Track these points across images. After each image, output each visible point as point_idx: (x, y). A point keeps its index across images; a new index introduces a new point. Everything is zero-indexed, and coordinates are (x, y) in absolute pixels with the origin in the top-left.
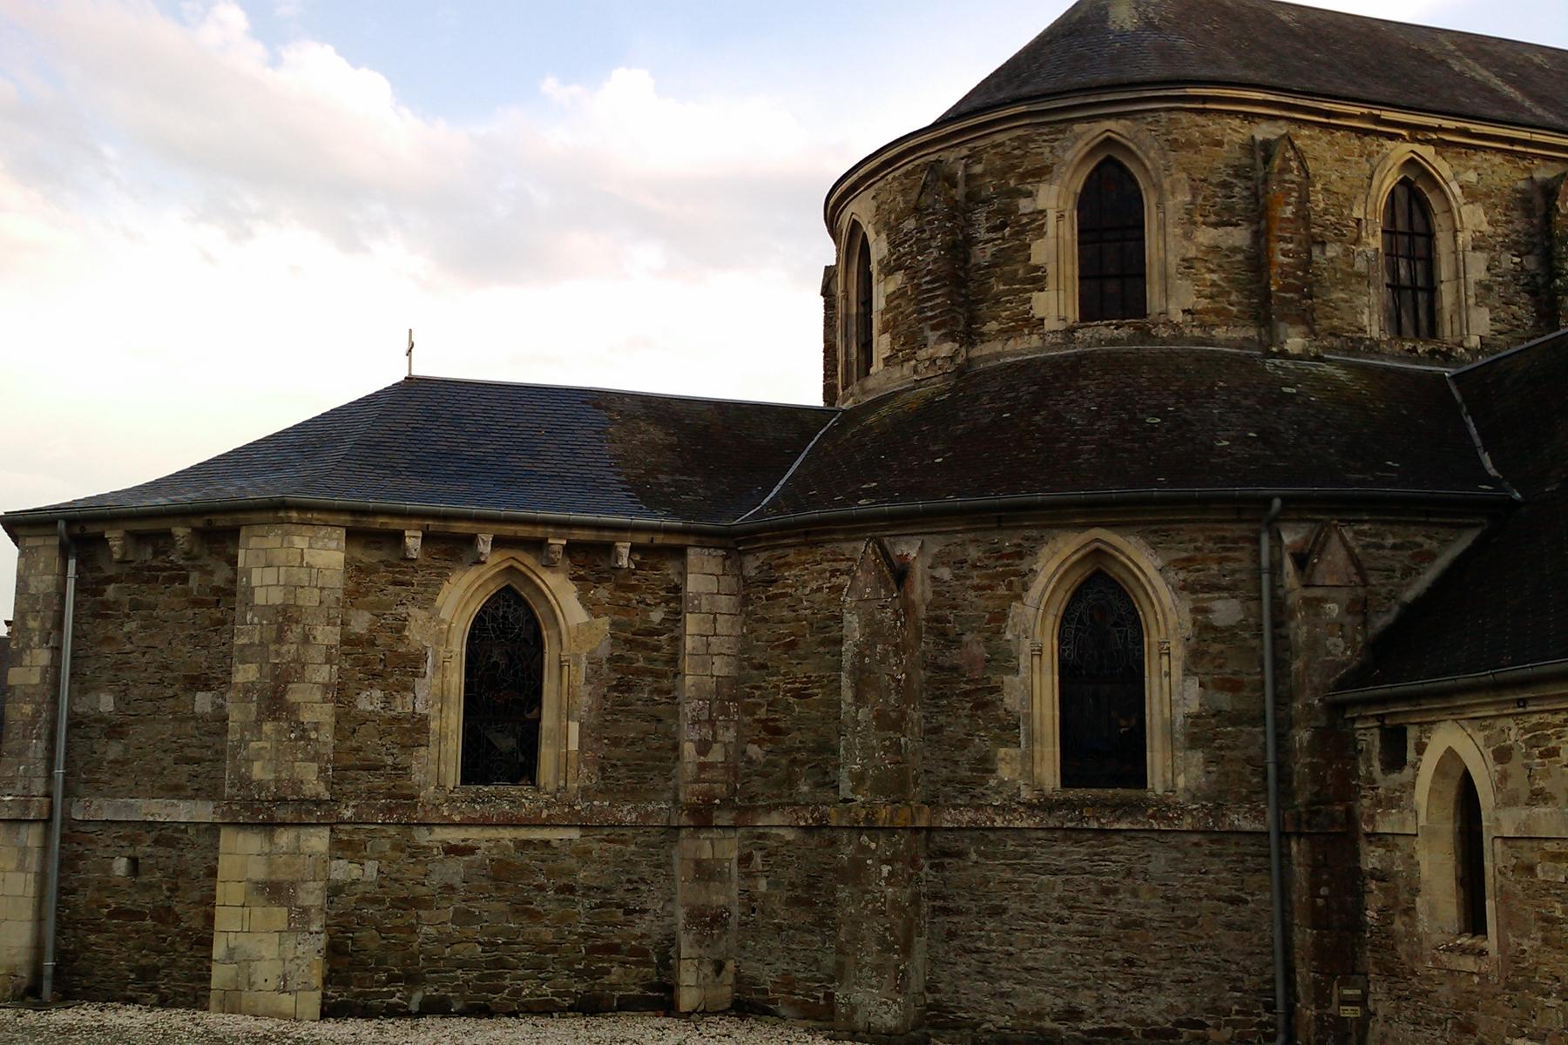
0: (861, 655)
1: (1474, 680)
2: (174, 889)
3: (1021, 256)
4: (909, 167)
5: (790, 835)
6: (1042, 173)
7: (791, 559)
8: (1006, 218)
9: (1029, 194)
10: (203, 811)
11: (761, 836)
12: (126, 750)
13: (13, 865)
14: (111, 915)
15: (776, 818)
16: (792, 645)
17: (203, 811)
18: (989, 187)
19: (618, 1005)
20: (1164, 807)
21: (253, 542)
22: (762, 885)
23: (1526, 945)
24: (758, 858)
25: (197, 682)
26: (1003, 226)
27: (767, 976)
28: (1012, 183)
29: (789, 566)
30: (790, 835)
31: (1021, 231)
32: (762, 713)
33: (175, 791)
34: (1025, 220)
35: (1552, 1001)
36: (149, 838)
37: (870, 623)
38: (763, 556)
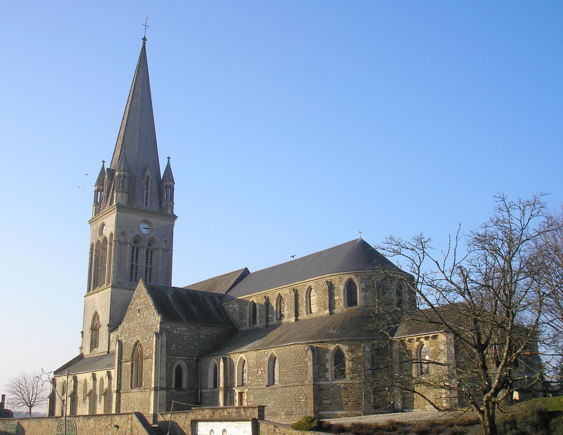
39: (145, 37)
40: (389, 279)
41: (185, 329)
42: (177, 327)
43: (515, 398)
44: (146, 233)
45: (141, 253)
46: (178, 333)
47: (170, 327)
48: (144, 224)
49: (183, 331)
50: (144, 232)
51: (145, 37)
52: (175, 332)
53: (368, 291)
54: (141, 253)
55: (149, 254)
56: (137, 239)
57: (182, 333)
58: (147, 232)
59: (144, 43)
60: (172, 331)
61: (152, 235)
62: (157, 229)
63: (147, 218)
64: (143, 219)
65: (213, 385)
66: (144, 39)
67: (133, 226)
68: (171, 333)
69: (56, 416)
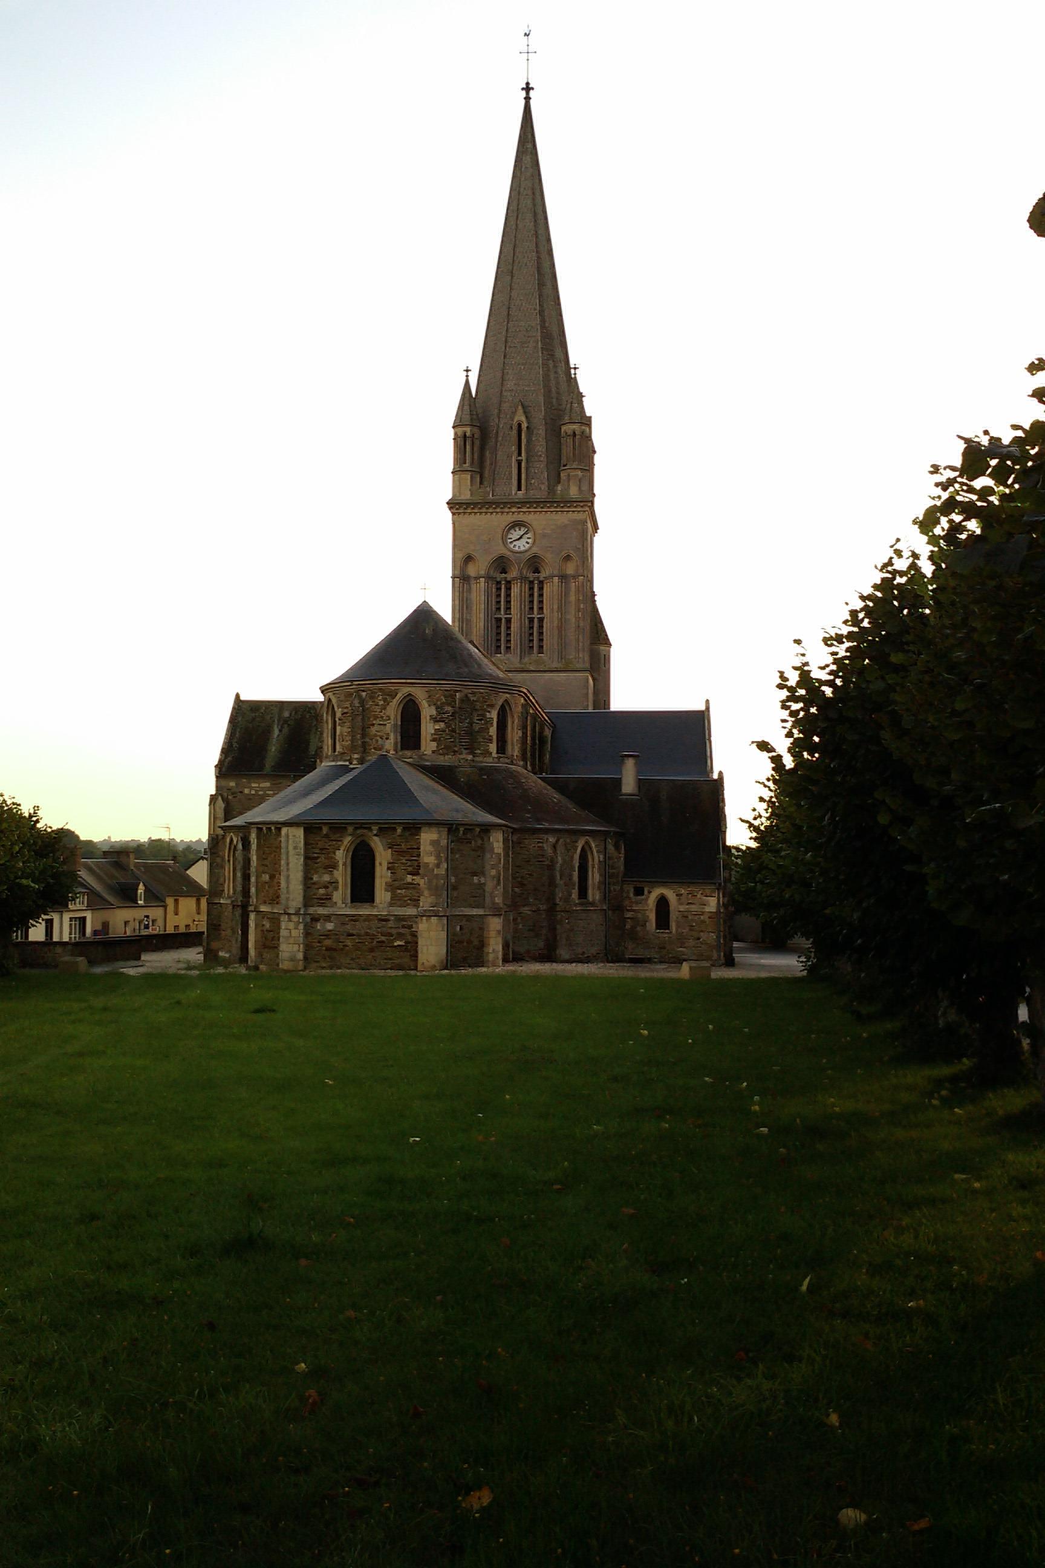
0: (561, 867)
1: (596, 870)
2: (471, 934)
3: (487, 731)
4: (449, 689)
5: (529, 913)
6: (492, 706)
7: (527, 837)
8: (482, 717)
9: (489, 712)
10: (481, 912)
11: (520, 913)
12: (458, 894)
13: (441, 929)
14: (456, 943)
15: (526, 908)
16: (528, 861)
17: (481, 912)
18: (478, 705)
19: (513, 958)
20: (592, 904)
21: (494, 834)
22: (520, 926)
23: (683, 931)
24: (519, 920)
25: (475, 874)
26: (481, 720)
27: (522, 950)
28: (485, 707)
29: (525, 839)
30: (529, 913)
31: (487, 723)
32: (519, 879)
33: (471, 906)
34: (488, 720)
35: (691, 941)
36: (464, 919)
37: (563, 859)
38: (519, 835)
39: (528, 84)
40: (380, 698)
41: (268, 784)
42: (250, 783)
43: (435, 860)
44: (524, 549)
45: (514, 592)
46: (253, 792)
47: (236, 784)
48: (517, 530)
49: (262, 789)
50: (519, 547)
51: (528, 84)
52: (246, 791)
53: (346, 724)
54: (514, 592)
55: (535, 587)
56: (501, 564)
57: (261, 793)
58: (528, 540)
59: (527, 99)
60: (241, 790)
61: (535, 550)
62: (544, 536)
63: (521, 517)
64: (513, 520)
65: (206, 877)
66: (528, 88)
67: (490, 539)
68: (239, 794)
69: (169, 932)
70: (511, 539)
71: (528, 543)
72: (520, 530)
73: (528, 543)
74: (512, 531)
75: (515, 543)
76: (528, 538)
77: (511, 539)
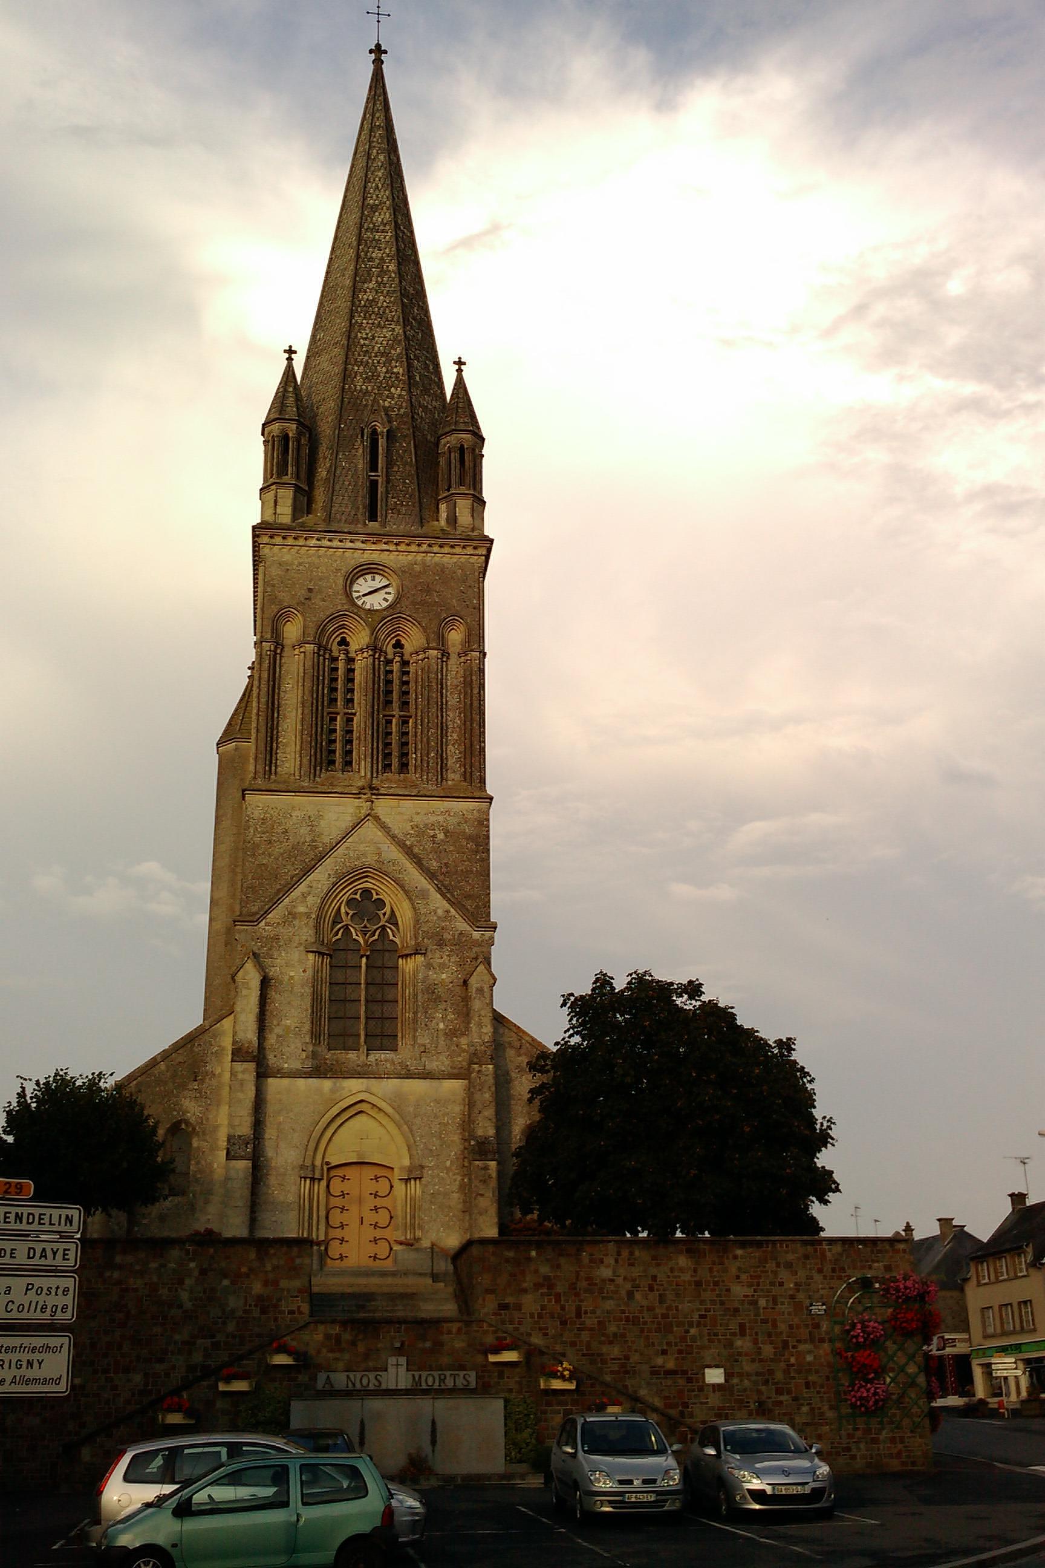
39: (378, 46)
51: (378, 46)
70: (358, 592)
71: (386, 600)
72: (373, 580)
73: (386, 600)
74: (361, 580)
75: (364, 599)
76: (386, 593)
77: (358, 592)
